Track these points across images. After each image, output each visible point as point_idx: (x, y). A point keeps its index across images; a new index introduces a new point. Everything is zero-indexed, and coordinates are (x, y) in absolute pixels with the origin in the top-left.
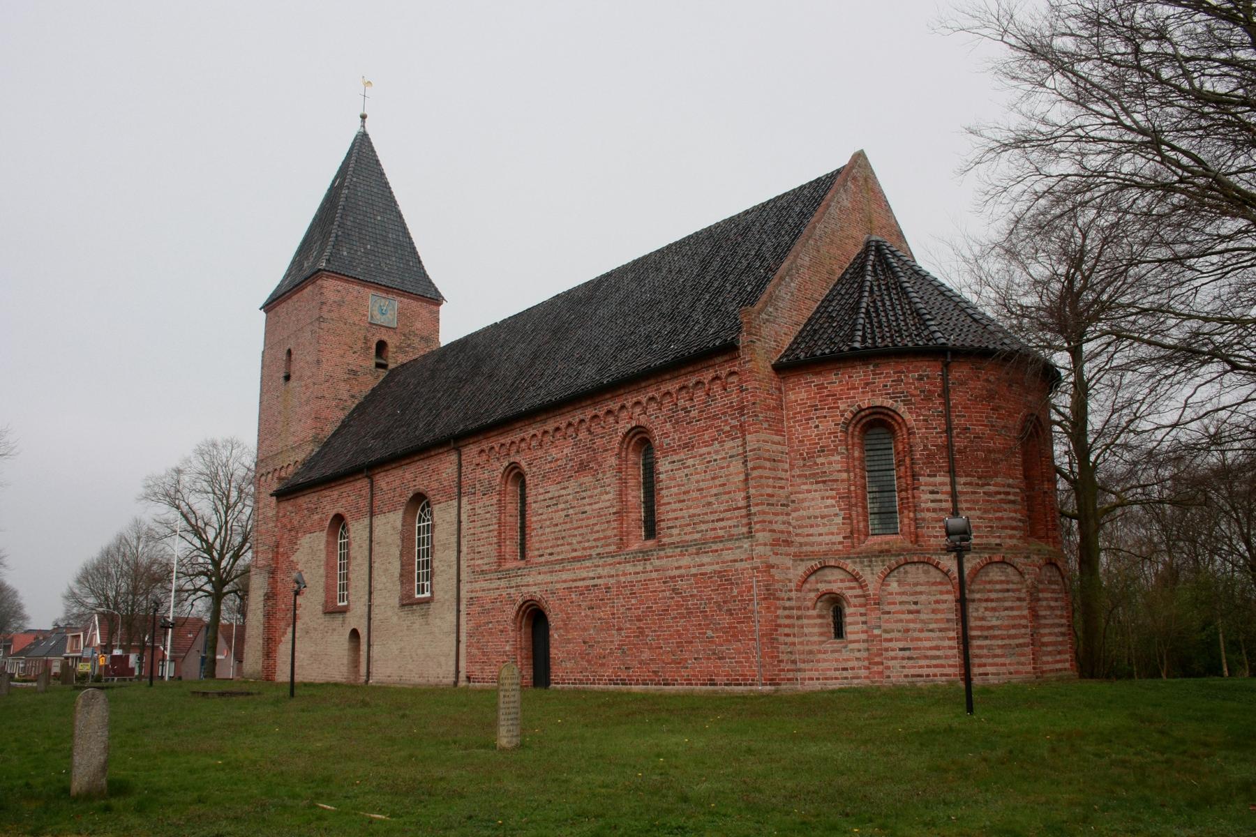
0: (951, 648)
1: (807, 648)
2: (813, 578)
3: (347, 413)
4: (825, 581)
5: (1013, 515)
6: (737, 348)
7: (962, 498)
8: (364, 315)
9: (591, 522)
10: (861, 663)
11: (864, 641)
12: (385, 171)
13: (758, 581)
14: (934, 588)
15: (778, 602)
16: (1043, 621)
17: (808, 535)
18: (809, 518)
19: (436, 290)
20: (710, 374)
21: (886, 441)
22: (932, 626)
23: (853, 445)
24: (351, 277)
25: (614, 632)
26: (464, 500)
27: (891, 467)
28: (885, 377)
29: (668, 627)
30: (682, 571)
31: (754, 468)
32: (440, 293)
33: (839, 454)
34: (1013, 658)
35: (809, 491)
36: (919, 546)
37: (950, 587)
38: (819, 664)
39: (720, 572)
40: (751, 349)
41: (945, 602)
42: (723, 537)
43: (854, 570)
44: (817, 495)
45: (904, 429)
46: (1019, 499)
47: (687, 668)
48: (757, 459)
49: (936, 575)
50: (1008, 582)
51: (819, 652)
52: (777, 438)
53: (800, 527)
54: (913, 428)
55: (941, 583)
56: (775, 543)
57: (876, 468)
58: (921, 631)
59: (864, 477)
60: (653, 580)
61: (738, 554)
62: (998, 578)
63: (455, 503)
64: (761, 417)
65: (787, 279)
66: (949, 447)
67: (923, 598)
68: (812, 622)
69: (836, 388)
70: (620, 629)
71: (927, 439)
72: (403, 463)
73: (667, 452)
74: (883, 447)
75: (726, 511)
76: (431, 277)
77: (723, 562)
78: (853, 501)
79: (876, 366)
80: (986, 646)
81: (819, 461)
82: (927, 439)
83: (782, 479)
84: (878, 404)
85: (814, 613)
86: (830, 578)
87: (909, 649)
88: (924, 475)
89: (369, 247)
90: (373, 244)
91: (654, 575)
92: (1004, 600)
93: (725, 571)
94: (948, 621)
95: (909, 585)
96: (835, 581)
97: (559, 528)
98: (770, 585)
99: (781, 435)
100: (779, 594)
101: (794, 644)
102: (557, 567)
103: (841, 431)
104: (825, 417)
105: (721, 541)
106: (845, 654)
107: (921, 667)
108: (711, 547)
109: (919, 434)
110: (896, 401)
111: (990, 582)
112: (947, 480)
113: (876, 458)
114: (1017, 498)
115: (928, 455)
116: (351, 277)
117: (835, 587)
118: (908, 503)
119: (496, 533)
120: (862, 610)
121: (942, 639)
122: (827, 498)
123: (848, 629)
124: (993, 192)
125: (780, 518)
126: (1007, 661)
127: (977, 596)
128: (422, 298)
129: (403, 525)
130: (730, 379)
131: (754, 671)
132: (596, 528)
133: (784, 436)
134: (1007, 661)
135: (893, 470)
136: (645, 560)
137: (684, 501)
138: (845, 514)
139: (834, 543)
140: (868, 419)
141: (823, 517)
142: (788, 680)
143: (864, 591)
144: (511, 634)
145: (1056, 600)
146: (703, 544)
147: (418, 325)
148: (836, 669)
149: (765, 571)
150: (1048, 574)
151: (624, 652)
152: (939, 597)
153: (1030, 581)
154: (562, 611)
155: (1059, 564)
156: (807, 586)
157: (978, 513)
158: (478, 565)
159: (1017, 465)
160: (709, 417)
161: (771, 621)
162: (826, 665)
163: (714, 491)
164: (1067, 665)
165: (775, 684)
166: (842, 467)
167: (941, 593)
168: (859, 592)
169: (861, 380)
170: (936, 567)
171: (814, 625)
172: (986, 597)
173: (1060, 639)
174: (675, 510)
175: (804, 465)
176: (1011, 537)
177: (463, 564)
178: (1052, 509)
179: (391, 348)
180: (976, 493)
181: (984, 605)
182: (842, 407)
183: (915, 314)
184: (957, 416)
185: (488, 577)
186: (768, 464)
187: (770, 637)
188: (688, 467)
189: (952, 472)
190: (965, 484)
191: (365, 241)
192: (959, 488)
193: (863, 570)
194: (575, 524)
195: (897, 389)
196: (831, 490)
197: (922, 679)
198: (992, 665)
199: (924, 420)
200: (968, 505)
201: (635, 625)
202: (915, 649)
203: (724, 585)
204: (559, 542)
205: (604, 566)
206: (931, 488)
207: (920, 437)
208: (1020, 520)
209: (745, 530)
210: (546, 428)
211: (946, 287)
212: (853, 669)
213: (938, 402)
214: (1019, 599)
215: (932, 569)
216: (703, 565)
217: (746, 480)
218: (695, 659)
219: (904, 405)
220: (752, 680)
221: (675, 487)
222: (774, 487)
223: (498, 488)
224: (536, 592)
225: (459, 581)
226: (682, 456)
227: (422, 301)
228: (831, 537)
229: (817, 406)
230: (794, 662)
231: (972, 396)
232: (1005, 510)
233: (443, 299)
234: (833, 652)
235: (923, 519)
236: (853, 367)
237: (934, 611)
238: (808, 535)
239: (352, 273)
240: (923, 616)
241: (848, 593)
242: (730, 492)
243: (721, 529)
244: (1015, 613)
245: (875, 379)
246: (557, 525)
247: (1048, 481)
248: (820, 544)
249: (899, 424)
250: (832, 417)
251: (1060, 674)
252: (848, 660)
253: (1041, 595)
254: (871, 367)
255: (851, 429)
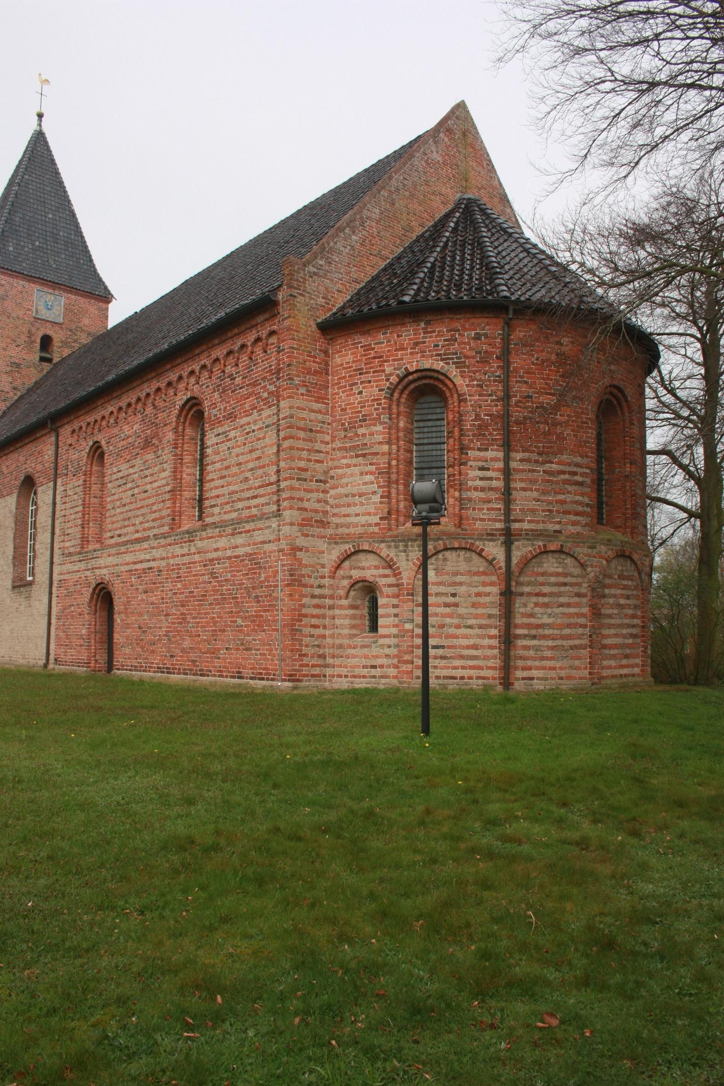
0: (491, 647)
1: (338, 642)
2: (346, 564)
3: (8, 404)
4: (359, 568)
5: (578, 498)
6: (275, 304)
7: (517, 476)
8: (29, 310)
9: (151, 501)
10: (390, 661)
11: (395, 636)
12: (61, 171)
13: (283, 565)
14: (476, 578)
15: (304, 589)
16: (607, 621)
17: (345, 516)
18: (347, 496)
19: (106, 288)
20: (252, 336)
21: (438, 410)
22: (470, 622)
23: (398, 414)
24: (15, 271)
25: (163, 618)
26: (59, 481)
27: (442, 440)
28: (436, 336)
29: (206, 614)
30: (220, 554)
31: (285, 439)
32: (109, 291)
33: (381, 423)
34: (565, 660)
35: (348, 466)
36: (462, 530)
37: (494, 578)
38: (349, 660)
39: (251, 555)
40: (290, 304)
41: (488, 594)
42: (256, 516)
43: (388, 555)
44: (356, 470)
45: (455, 396)
46: (588, 480)
47: (219, 658)
48: (289, 427)
49: (479, 564)
50: (565, 575)
51: (349, 647)
52: (316, 406)
53: (338, 506)
54: (465, 394)
55: (484, 573)
56: (305, 523)
57: (426, 441)
58: (458, 627)
59: (411, 452)
60: (195, 562)
61: (267, 535)
62: (552, 570)
63: (51, 484)
64: (297, 381)
65: (347, 231)
66: (505, 417)
67: (463, 589)
68: (344, 612)
69: (383, 348)
70: (167, 615)
71: (480, 407)
72: (18, 446)
73: (214, 425)
74: (434, 417)
75: (260, 487)
76: (102, 275)
77: (254, 544)
78: (394, 477)
79: (428, 323)
80: (533, 646)
81: (361, 431)
82: (480, 407)
83: (320, 452)
84: (427, 366)
85: (344, 602)
86: (364, 564)
87: (443, 647)
88: (473, 449)
89: (37, 243)
90: (42, 240)
91: (197, 558)
92: (560, 595)
93: (255, 553)
94: (490, 616)
95: (447, 574)
96: (369, 568)
97: (127, 508)
98: (295, 570)
99: (323, 403)
100: (306, 580)
101: (324, 637)
102: (123, 549)
103: (385, 398)
104: (370, 382)
105: (253, 521)
106: (375, 651)
107: (455, 668)
108: (244, 527)
109: (470, 401)
110: (448, 364)
111: (543, 574)
112: (500, 455)
113: (426, 430)
114: (585, 479)
115: (480, 425)
116: (15, 271)
117: (368, 574)
118: (454, 481)
119: (80, 515)
120: (395, 601)
121: (482, 637)
122: (366, 474)
123: (381, 621)
124: (552, 101)
125: (314, 495)
126: (558, 664)
127: (527, 589)
128: (90, 295)
129: (17, 509)
130: (271, 341)
131: (276, 665)
132: (155, 508)
133: (328, 404)
134: (558, 664)
135: (444, 443)
136: (190, 541)
137: (224, 477)
138: (383, 492)
139: (370, 525)
140: (416, 384)
141: (360, 495)
142: (313, 676)
143: (398, 580)
144: (87, 617)
145: (628, 597)
146: (238, 523)
147: (86, 321)
148: (365, 667)
149: (290, 554)
150: (620, 568)
151: (170, 640)
152: (481, 589)
153: (592, 574)
154: (124, 594)
155: (635, 557)
156: (340, 572)
157: (535, 494)
158: (67, 548)
159: (588, 442)
160: (251, 384)
161: (294, 610)
162: (354, 661)
163: (251, 465)
164: (637, 670)
165: (293, 681)
166: (383, 438)
167: (484, 584)
168: (392, 580)
169: (410, 339)
170: (480, 554)
171: (346, 616)
172: (537, 591)
173: (630, 641)
174: (216, 488)
175: (345, 436)
176: (574, 523)
177: (56, 546)
178: (634, 495)
179: (56, 343)
180: (534, 471)
181: (534, 599)
182: (388, 370)
183: (484, 268)
184: (517, 382)
185: (73, 558)
186: (302, 434)
187: (293, 628)
188: (230, 439)
189: (507, 447)
190: (521, 460)
191: (33, 238)
192: (513, 465)
193: (397, 556)
194: (139, 504)
195: (449, 349)
196: (371, 464)
197: (455, 681)
198: (538, 668)
199: (478, 385)
200: (523, 485)
201: (179, 610)
202: (449, 647)
203: (254, 569)
204: (126, 523)
205: (158, 548)
206: (480, 464)
207: (472, 405)
208: (587, 505)
209: (275, 508)
210: (120, 404)
211: (530, 244)
212: (382, 666)
213: (496, 365)
214: (578, 595)
215: (474, 556)
216: (237, 547)
217: (278, 451)
218: (227, 649)
219: (457, 368)
220: (274, 675)
221: (218, 461)
222: (309, 460)
223: (84, 468)
224: (104, 573)
225: (52, 563)
226: (226, 428)
227: (91, 298)
228: (367, 517)
229: (362, 369)
230: (323, 656)
231: (537, 359)
232: (569, 493)
233: (112, 296)
234: (363, 647)
235: (470, 500)
236: (403, 324)
237: (474, 605)
238: (345, 516)
239: (17, 268)
240: (461, 610)
241: (382, 581)
242: (264, 467)
243: (255, 507)
244: (572, 610)
245: (426, 337)
246: (125, 505)
247: (631, 463)
248: (356, 525)
249: (450, 389)
250: (377, 381)
251: (625, 680)
252: (377, 657)
253: (607, 591)
254: (422, 325)
255: (396, 395)
